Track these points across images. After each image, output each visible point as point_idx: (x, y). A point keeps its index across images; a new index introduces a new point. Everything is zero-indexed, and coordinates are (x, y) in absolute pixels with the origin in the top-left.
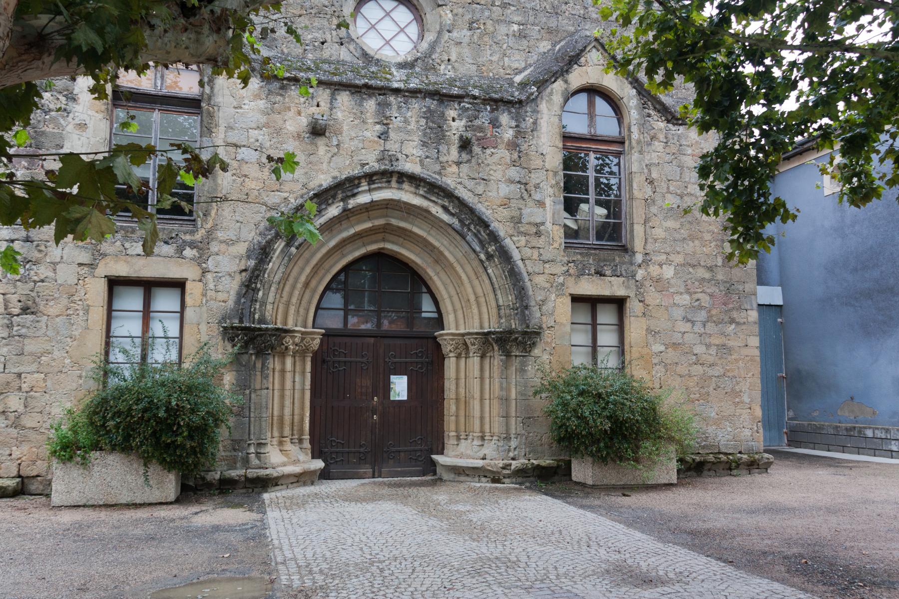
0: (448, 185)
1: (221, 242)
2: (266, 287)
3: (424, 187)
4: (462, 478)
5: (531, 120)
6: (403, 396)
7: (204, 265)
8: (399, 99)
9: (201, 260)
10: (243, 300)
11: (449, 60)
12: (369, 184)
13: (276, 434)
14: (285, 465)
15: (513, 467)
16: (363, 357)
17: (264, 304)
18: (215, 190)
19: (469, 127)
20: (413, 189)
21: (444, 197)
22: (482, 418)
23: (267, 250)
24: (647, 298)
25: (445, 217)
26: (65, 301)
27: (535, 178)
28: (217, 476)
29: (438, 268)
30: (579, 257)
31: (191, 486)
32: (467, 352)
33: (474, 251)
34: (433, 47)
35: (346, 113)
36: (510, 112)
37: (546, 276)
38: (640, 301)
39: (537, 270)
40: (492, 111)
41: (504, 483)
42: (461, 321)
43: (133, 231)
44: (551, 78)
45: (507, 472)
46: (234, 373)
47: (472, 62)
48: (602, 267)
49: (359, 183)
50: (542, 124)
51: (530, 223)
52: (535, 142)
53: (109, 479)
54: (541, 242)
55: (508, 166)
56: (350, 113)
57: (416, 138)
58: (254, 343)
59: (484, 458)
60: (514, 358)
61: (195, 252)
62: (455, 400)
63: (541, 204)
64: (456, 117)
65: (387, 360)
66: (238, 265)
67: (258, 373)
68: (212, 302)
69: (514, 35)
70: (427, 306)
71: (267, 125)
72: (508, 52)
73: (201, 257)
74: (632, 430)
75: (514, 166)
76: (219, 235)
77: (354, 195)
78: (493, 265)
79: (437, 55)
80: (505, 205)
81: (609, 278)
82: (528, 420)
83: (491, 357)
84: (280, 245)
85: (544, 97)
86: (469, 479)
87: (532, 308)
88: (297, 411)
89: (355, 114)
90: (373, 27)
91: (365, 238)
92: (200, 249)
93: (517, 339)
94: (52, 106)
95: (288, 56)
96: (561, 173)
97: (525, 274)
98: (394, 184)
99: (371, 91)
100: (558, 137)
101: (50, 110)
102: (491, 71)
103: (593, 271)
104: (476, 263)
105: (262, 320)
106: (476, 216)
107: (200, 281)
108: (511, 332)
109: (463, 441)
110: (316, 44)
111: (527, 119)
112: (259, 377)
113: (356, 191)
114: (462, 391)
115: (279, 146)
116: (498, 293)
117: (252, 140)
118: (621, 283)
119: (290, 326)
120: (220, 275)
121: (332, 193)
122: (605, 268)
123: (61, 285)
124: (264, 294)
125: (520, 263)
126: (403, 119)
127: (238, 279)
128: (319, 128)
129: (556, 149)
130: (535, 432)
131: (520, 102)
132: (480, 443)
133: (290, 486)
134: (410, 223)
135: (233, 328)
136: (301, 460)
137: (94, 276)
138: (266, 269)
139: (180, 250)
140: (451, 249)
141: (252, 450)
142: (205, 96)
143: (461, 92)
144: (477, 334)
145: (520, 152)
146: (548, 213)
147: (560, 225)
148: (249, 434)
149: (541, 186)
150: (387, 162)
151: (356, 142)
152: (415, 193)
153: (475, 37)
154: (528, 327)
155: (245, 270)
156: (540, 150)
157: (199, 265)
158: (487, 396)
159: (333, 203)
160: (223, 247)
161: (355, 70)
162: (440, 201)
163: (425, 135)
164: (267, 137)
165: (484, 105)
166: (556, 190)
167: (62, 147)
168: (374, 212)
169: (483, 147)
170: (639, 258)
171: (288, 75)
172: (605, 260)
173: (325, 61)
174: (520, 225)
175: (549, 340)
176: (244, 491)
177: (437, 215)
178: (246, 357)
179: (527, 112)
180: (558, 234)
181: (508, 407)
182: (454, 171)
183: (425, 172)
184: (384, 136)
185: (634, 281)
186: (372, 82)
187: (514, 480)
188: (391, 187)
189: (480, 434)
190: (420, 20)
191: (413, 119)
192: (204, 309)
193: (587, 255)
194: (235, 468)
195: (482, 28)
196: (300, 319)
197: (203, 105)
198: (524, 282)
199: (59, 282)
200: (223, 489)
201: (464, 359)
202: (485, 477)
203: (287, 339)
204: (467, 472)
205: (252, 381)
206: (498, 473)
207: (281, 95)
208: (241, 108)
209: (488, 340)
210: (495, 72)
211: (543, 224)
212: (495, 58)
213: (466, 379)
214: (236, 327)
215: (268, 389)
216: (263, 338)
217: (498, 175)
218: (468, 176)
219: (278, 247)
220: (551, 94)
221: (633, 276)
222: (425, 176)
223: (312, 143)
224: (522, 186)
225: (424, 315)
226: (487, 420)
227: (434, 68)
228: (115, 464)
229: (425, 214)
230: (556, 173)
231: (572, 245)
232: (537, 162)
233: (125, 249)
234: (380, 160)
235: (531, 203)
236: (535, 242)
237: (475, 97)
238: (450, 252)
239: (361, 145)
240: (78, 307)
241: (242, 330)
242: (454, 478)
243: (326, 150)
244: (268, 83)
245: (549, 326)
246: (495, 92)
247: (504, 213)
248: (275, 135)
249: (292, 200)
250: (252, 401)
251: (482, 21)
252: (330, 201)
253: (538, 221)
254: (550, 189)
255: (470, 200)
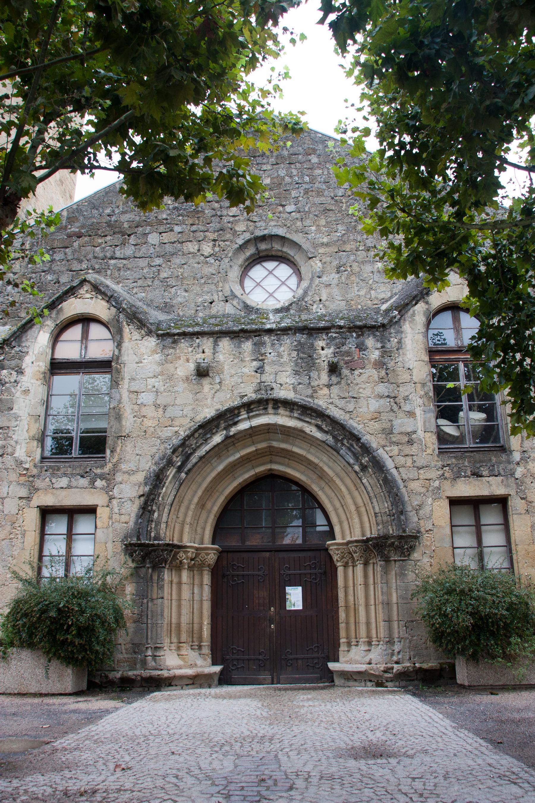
0: (320, 406)
1: (124, 473)
2: (161, 509)
3: (298, 410)
4: (351, 683)
5: (396, 340)
6: (298, 606)
7: (111, 493)
8: (273, 338)
9: (108, 489)
10: (140, 521)
11: (320, 300)
12: (248, 413)
13: (175, 640)
14: (181, 668)
15: (394, 671)
16: (259, 570)
17: (158, 523)
18: (120, 430)
19: (337, 353)
20: (288, 413)
21: (316, 417)
22: (368, 624)
23: (161, 477)
24: (528, 495)
25: (319, 435)
26: (8, 528)
27: (403, 391)
28: (119, 675)
29: (323, 484)
30: (454, 460)
31: (96, 683)
32: (354, 561)
33: (348, 463)
34: (306, 293)
35: (227, 355)
36: (375, 336)
37: (421, 481)
38: (522, 499)
39: (411, 477)
40: (358, 336)
41: (387, 687)
42: (347, 532)
43: (58, 469)
44: (411, 301)
45: (390, 675)
46: (134, 584)
47: (341, 299)
48: (479, 468)
49: (239, 413)
50: (407, 343)
51: (401, 433)
52: (401, 359)
53: (22, 671)
54: (414, 449)
55: (376, 383)
56: (230, 355)
57: (289, 369)
58: (149, 558)
59: (370, 663)
60: (393, 562)
61: (104, 483)
62: (344, 608)
63: (411, 414)
64: (324, 346)
65: (282, 572)
66: (138, 492)
67: (155, 585)
68: (117, 524)
69: (379, 272)
70: (320, 520)
71: (162, 373)
72: (374, 286)
73: (108, 486)
74: (498, 626)
75: (382, 382)
76: (123, 467)
77: (235, 424)
78: (368, 475)
79: (309, 298)
80: (376, 418)
81: (486, 478)
82: (409, 624)
83: (374, 563)
84: (171, 472)
85: (407, 319)
86: (356, 684)
87: (409, 513)
88: (196, 620)
89: (234, 355)
90: (258, 284)
91: (253, 462)
92: (108, 480)
93: (393, 543)
94: (7, 380)
95: (183, 317)
96: (430, 386)
97: (400, 481)
98: (270, 410)
99: (248, 334)
100: (424, 352)
101: (6, 383)
102: (359, 304)
103: (469, 473)
104: (353, 475)
105: (157, 538)
106: (347, 431)
107: (108, 506)
108: (386, 537)
109: (353, 647)
110: (206, 304)
111: (392, 339)
112: (155, 588)
113: (236, 420)
114: (351, 598)
115: (171, 389)
116: (374, 500)
117: (150, 387)
118: (500, 482)
119: (186, 542)
120: (123, 500)
121: (215, 423)
122: (482, 469)
123: (6, 515)
124: (159, 515)
125: (394, 471)
126: (276, 354)
127: (138, 503)
128: (202, 370)
129: (422, 363)
130: (419, 635)
131: (383, 326)
132: (367, 648)
133: (185, 687)
134: (291, 444)
135: (131, 545)
136: (199, 665)
137: (30, 507)
138: (160, 493)
139: (92, 482)
140: (331, 464)
141: (149, 653)
142: (115, 357)
143: (327, 324)
144: (356, 541)
145: (387, 369)
146: (419, 422)
147: (432, 432)
148: (147, 639)
149: (410, 397)
150: (263, 392)
151: (236, 378)
152: (290, 416)
153: (343, 278)
154: (404, 531)
155: (143, 495)
156: (407, 366)
157: (107, 493)
158: (372, 602)
159: (217, 432)
160: (126, 476)
161: (237, 320)
162: (313, 421)
163: (296, 365)
164: (161, 383)
165: (350, 332)
166: (425, 400)
167: (12, 409)
168: (256, 437)
169: (351, 369)
170: (517, 456)
171: (178, 331)
172: (480, 462)
173: (212, 317)
174: (391, 436)
175: (428, 543)
176: (141, 689)
177: (311, 433)
178: (143, 570)
179: (391, 333)
180: (431, 441)
181: (390, 611)
182: (325, 393)
183: (298, 397)
184: (260, 370)
185: (513, 479)
186: (248, 327)
187: (397, 684)
188: (268, 414)
189: (366, 640)
190: (298, 273)
191: (286, 353)
192: (111, 529)
193: (462, 458)
194: (135, 669)
195: (349, 270)
196: (198, 537)
197: (113, 364)
198: (398, 489)
199: (5, 513)
200: (122, 687)
201: (351, 568)
202: (370, 681)
203: (181, 554)
204: (354, 677)
205: (149, 591)
206: (381, 676)
207: (173, 348)
208: (141, 362)
209: (369, 548)
210: (363, 304)
211: (415, 432)
212: (362, 293)
213: (354, 586)
214: (133, 544)
215: (162, 598)
216: (156, 553)
217: (367, 392)
218: (338, 396)
219: (170, 473)
220: (413, 315)
221: (512, 474)
222: (297, 400)
223: (198, 384)
224: (392, 400)
225: (319, 529)
226: (373, 625)
227: (307, 309)
228: (27, 659)
229: (301, 434)
230: (424, 385)
231: (448, 450)
232: (404, 377)
233: (52, 484)
234: (256, 391)
235: (401, 415)
236: (407, 450)
237: (340, 327)
238: (329, 467)
239: (240, 380)
240: (18, 532)
241: (138, 546)
242: (344, 683)
243: (210, 388)
244: (163, 340)
245: (427, 529)
246: (360, 321)
247: (376, 426)
248: (168, 380)
249: (182, 433)
250: (149, 609)
251: (348, 265)
252: (214, 431)
253: (409, 430)
254: (419, 400)
255: (342, 417)
